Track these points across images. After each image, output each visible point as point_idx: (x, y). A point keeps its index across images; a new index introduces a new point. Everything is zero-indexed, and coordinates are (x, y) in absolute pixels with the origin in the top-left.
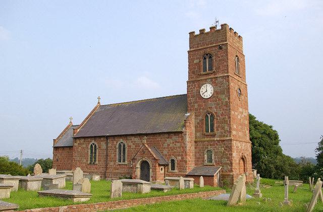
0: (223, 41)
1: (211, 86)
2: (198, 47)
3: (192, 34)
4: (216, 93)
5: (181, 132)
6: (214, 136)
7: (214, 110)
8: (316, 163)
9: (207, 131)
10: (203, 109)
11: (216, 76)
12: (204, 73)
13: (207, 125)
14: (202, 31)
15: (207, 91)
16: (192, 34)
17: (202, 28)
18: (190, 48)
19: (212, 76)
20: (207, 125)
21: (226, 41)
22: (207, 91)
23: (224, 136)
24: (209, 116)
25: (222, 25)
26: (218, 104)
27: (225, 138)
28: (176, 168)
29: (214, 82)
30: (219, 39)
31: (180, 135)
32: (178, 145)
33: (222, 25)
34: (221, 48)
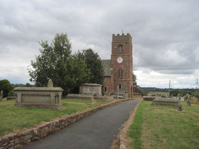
0: (127, 41)
1: (122, 58)
2: (116, 41)
3: (66, 35)
4: (124, 62)
5: (110, 76)
6: (122, 78)
7: (122, 68)
8: (80, 87)
9: (119, 76)
10: (118, 67)
11: (124, 54)
12: (119, 53)
13: (119, 74)
14: (118, 35)
15: (120, 60)
16: (113, 35)
17: (114, 34)
18: (113, 41)
19: (123, 54)
20: (119, 74)
21: (129, 41)
22: (120, 60)
23: (126, 79)
24: (120, 70)
25: (127, 34)
26: (124, 66)
27: (127, 80)
28: (107, 90)
29: (123, 57)
30: (126, 39)
31: (109, 77)
32: (108, 81)
33: (127, 34)
34: (127, 43)
